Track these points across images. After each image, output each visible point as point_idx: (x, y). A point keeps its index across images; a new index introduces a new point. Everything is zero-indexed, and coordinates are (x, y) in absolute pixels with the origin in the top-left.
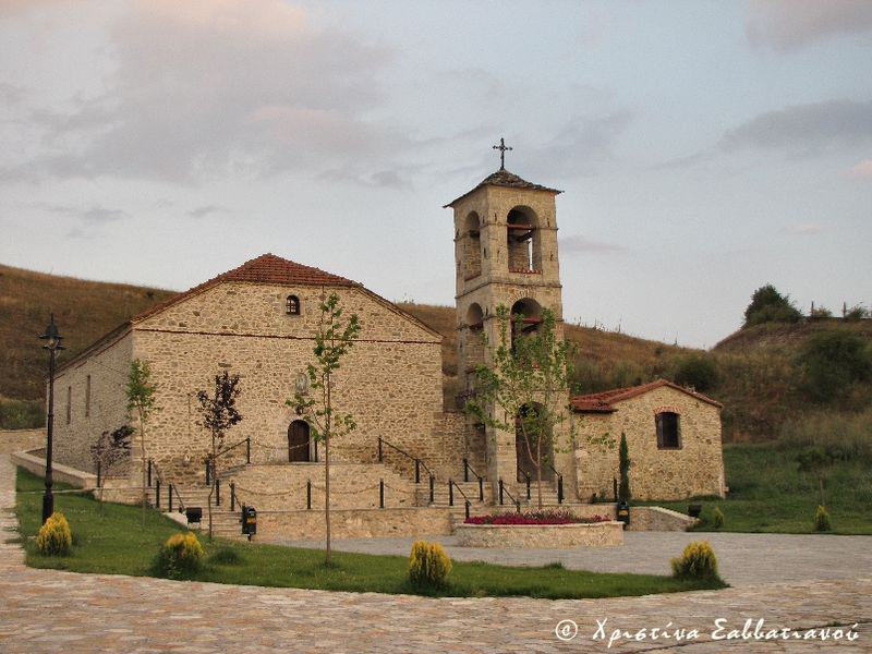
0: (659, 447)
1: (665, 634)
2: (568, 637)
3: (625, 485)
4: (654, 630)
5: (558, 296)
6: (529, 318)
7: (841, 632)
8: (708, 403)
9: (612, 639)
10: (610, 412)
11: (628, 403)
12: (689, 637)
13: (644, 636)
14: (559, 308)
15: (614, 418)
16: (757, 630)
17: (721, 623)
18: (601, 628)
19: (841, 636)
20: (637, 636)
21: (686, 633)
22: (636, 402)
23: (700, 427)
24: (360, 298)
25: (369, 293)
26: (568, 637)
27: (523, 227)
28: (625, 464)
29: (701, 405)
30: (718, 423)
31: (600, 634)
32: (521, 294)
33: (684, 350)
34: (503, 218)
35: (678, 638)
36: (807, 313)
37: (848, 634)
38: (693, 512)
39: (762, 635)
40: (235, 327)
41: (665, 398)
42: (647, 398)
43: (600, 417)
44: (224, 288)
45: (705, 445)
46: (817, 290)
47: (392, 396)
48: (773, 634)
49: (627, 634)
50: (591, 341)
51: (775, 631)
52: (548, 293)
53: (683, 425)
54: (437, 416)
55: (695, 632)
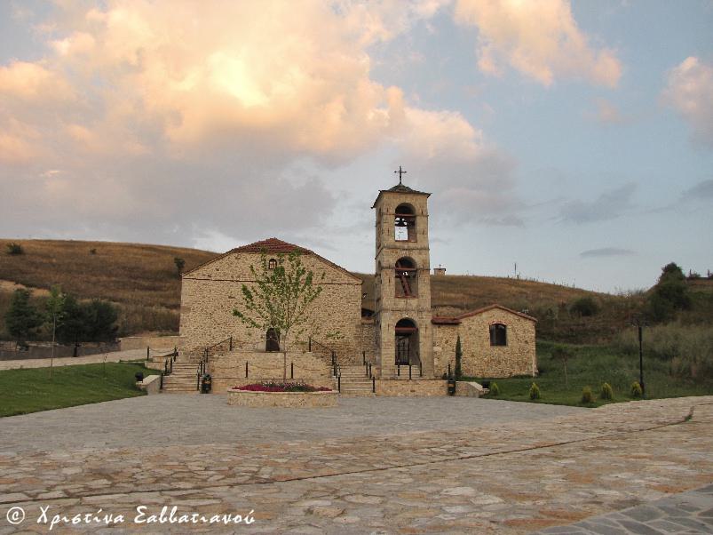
0: (492, 344)
1: (96, 518)
2: (18, 520)
3: (458, 367)
4: (88, 515)
5: (427, 255)
6: (407, 271)
7: (240, 517)
8: (526, 318)
9: (53, 523)
10: (457, 324)
11: (471, 318)
12: (116, 521)
13: (79, 520)
14: (426, 262)
15: (460, 328)
16: (172, 515)
17: (141, 510)
18: (44, 514)
19: (240, 520)
20: (74, 520)
21: (113, 518)
22: (477, 318)
23: (521, 334)
24: (313, 259)
25: (318, 257)
26: (18, 520)
27: (407, 215)
28: (459, 355)
29: (522, 320)
30: (534, 331)
31: (43, 519)
32: (403, 254)
33: (581, 291)
34: (393, 211)
35: (107, 522)
36: (687, 275)
37: (246, 519)
38: (485, 385)
39: (175, 519)
40: (239, 277)
41: (497, 316)
42: (484, 315)
43: (451, 327)
44: (233, 256)
45: (523, 344)
46: (697, 264)
47: (329, 315)
48: (185, 518)
49: (65, 519)
50: (442, 282)
51: (186, 517)
52: (420, 254)
53: (509, 333)
54: (357, 326)
55: (121, 517)
